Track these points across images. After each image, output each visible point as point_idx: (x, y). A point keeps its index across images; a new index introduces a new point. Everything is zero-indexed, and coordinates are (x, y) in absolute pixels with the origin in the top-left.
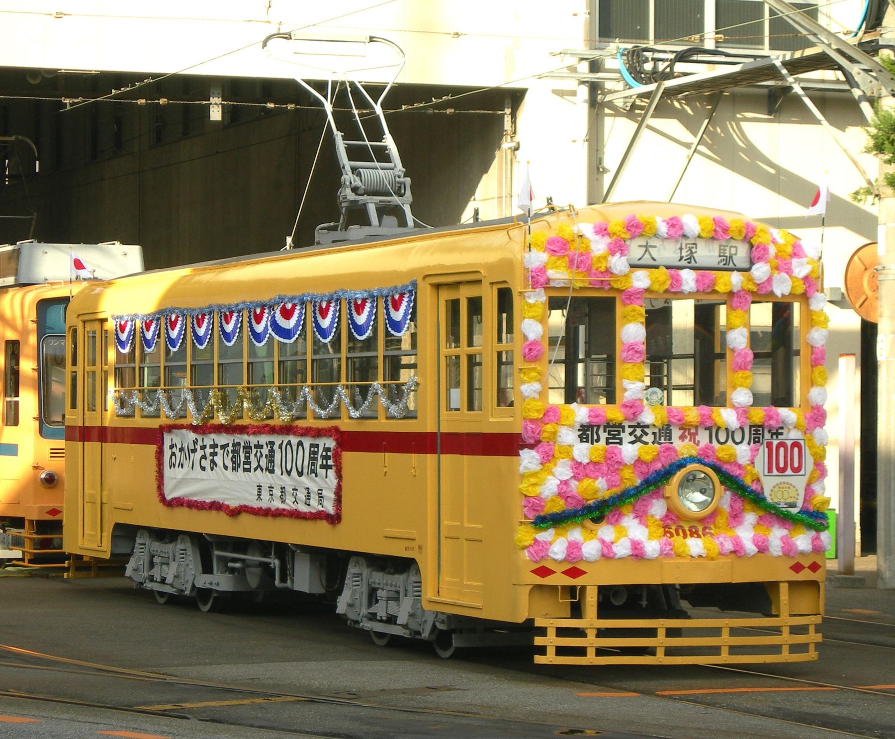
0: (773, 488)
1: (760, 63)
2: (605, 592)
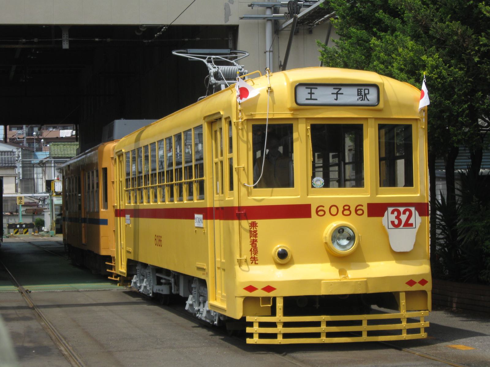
1: (58, 164)
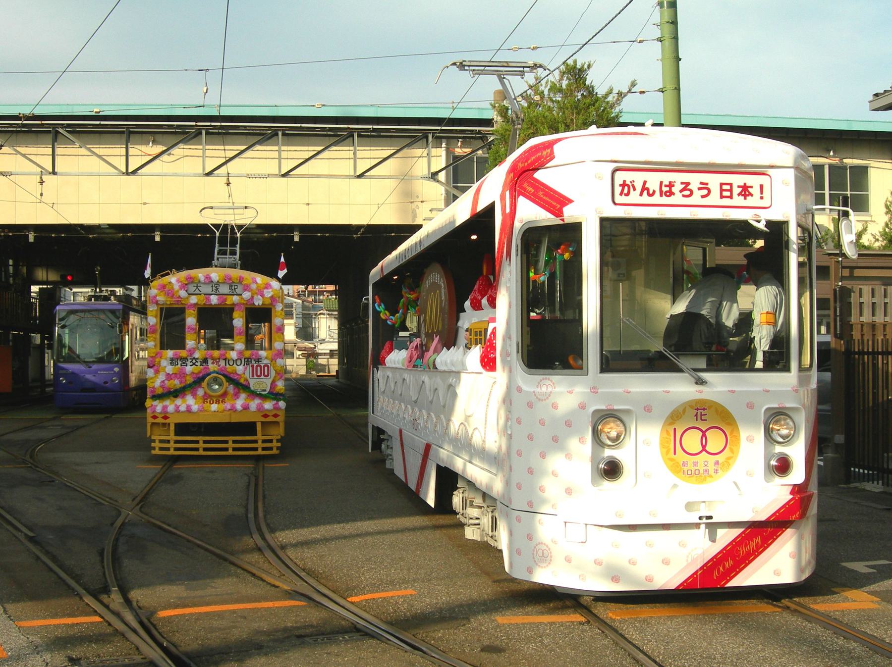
0: (254, 384)
2: (177, 425)
